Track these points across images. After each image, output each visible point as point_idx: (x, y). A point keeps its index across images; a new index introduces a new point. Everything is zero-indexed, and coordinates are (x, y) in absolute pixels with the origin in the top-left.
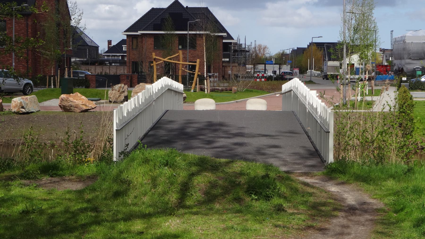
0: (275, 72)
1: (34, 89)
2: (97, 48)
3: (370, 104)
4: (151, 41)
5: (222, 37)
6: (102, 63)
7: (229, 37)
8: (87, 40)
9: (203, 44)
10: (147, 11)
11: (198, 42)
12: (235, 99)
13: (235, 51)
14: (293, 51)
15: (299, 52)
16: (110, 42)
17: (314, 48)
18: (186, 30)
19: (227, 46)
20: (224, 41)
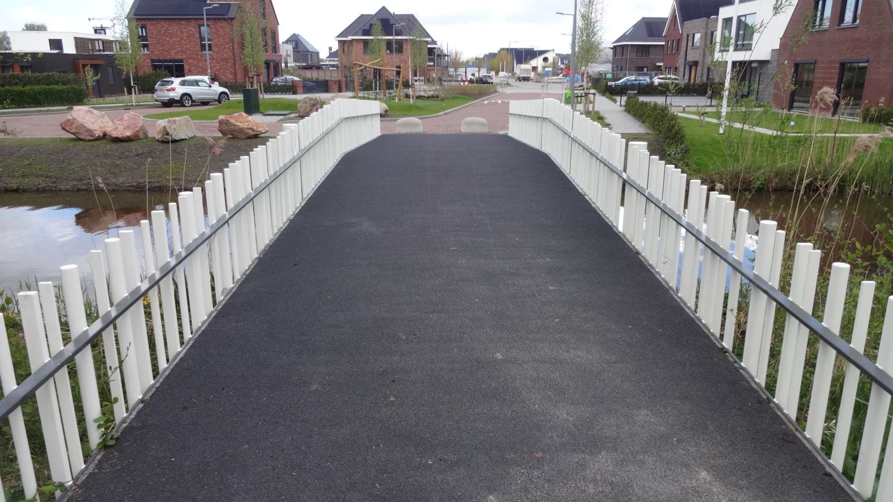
0: (473, 75)
1: (230, 96)
2: (318, 53)
3: (872, 154)
4: (361, 46)
5: (427, 43)
6: (319, 68)
7: (434, 42)
8: (308, 47)
9: (407, 48)
10: (842, 401)
11: (404, 47)
12: (443, 109)
13: (439, 56)
14: (486, 56)
15: (492, 56)
16: (330, 49)
17: (504, 52)
18: (392, 35)
19: (431, 51)
20: (429, 46)
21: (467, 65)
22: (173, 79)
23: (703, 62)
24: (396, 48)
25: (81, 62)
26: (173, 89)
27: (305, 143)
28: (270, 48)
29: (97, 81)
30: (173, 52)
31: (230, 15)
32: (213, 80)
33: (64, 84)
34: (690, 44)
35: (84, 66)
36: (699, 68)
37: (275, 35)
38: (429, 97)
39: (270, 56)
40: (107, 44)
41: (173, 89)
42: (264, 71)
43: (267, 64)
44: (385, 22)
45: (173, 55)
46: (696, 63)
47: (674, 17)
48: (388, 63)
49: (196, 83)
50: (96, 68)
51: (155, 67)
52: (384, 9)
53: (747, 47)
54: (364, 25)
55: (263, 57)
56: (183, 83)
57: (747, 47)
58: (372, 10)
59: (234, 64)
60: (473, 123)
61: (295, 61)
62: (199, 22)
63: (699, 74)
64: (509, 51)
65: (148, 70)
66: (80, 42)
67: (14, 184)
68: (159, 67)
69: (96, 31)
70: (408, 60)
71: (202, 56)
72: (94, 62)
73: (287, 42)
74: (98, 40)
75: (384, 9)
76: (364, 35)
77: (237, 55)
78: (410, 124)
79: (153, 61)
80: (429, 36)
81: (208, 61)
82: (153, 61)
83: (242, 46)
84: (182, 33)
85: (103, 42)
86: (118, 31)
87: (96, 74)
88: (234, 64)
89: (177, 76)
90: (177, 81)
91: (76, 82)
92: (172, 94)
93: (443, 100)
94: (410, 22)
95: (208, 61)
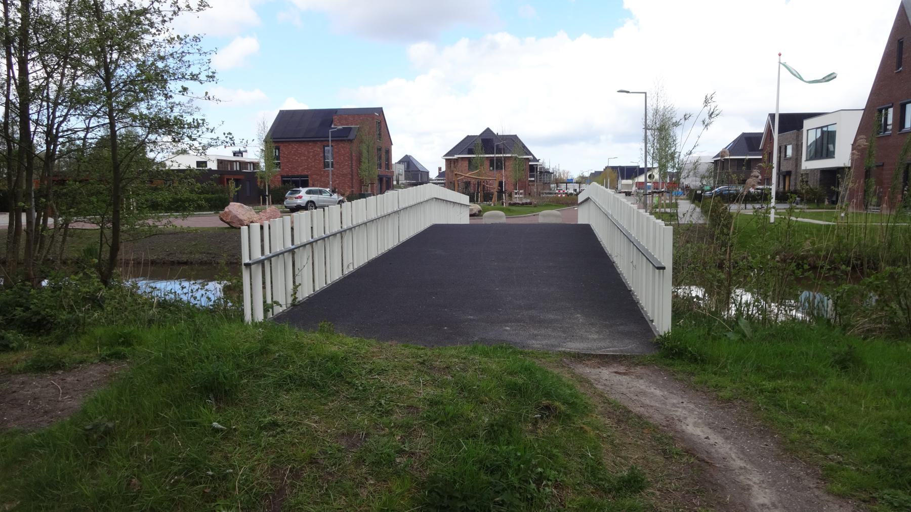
2: (428, 173)
4: (466, 163)
7: (535, 160)
16: (440, 169)
19: (532, 169)
21: (570, 181)
22: (301, 188)
23: (796, 172)
24: (497, 164)
25: (226, 177)
26: (300, 197)
27: (402, 206)
28: (383, 165)
29: (237, 191)
30: (300, 169)
31: (350, 137)
32: (334, 192)
33: (213, 193)
34: (783, 155)
35: (228, 180)
36: (793, 177)
37: (388, 152)
38: (523, 204)
39: (383, 171)
40: (243, 164)
41: (300, 197)
42: (376, 182)
43: (381, 179)
44: (488, 141)
45: (300, 171)
46: (789, 173)
47: (769, 132)
48: (492, 178)
49: (321, 192)
50: (237, 182)
51: (284, 182)
52: (488, 129)
53: (830, 155)
54: (468, 145)
55: (377, 172)
56: (308, 192)
57: (830, 155)
58: (477, 131)
59: (352, 179)
60: (549, 215)
61: (406, 179)
62: (325, 143)
63: (792, 183)
64: (614, 168)
65: (279, 185)
66: (220, 162)
67: (184, 258)
68: (288, 182)
69: (235, 154)
70: (506, 175)
71: (324, 172)
72: (236, 177)
73: (400, 162)
74: (236, 161)
75: (488, 129)
76: (469, 154)
77: (355, 171)
78: (495, 216)
79: (282, 177)
80: (531, 154)
81: (330, 176)
82: (282, 177)
83: (359, 161)
84: (309, 152)
85: (241, 163)
86: (254, 153)
87: (237, 186)
88: (352, 179)
89: (303, 186)
90: (303, 191)
91: (222, 192)
92: (299, 201)
93: (535, 206)
94: (513, 142)
95: (330, 176)
